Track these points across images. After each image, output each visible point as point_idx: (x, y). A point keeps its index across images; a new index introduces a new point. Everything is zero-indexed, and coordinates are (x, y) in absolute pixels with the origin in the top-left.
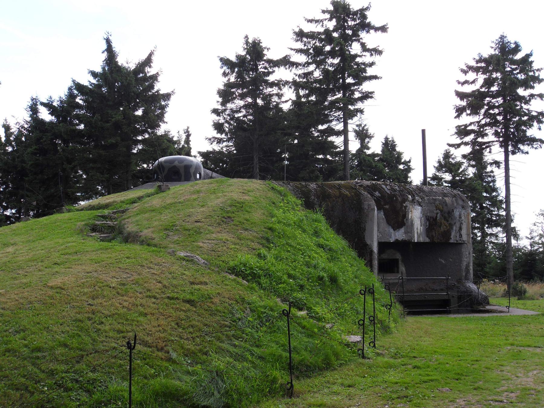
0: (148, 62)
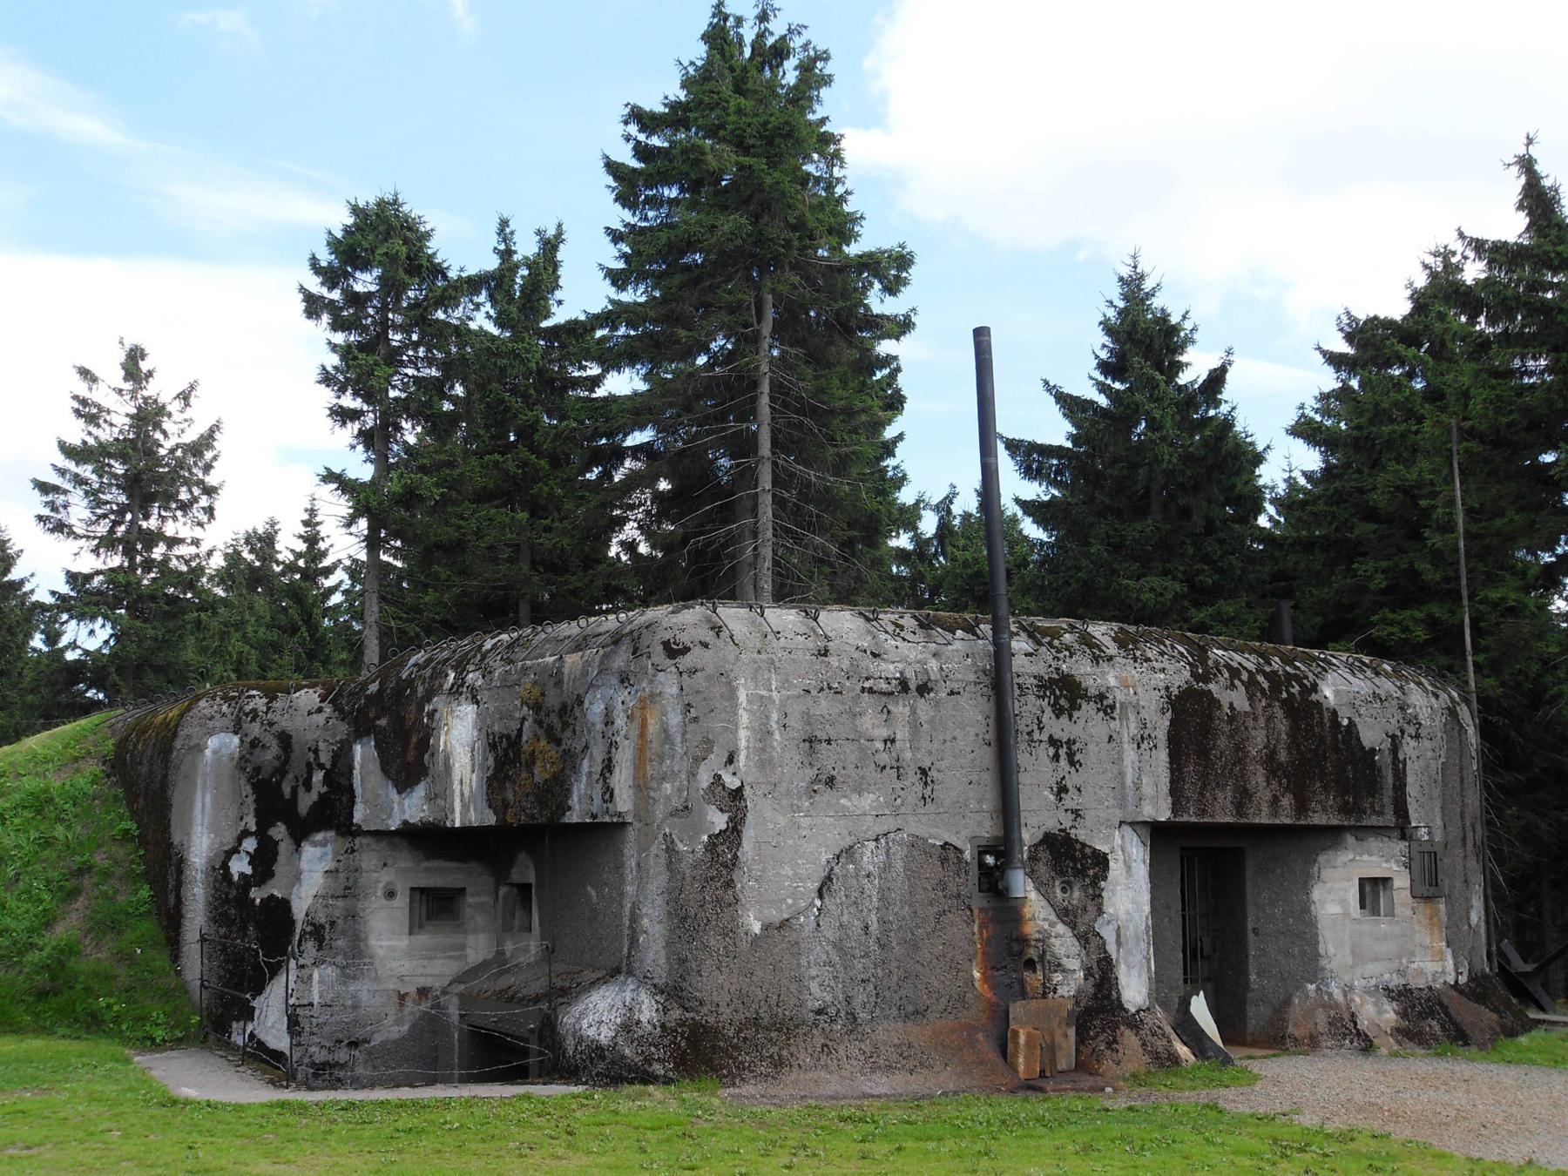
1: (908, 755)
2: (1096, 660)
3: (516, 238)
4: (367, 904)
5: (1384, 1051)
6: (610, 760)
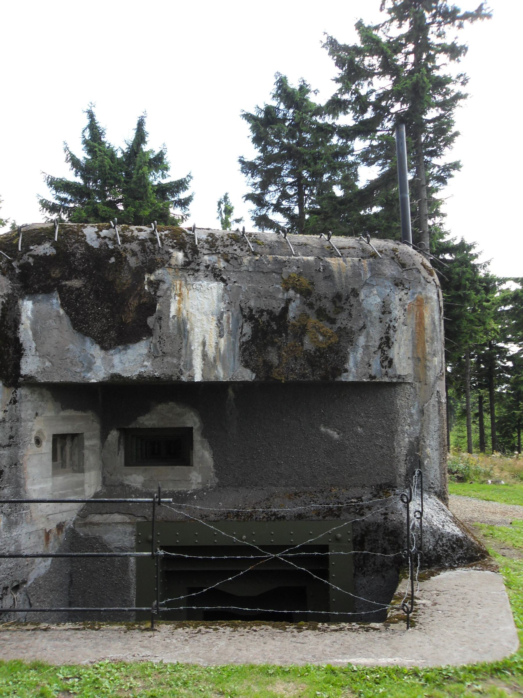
0: (141, 136)
4: (25, 451)
6: (388, 339)
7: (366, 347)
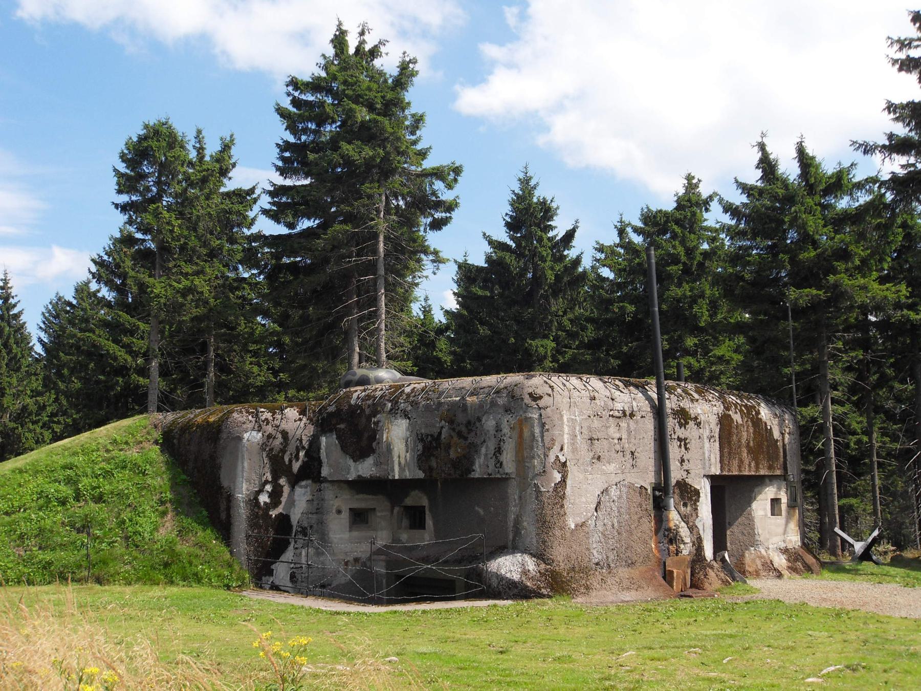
1: (627, 445)
2: (692, 400)
3: (206, 140)
5: (785, 577)
6: (500, 448)
7: (486, 455)
